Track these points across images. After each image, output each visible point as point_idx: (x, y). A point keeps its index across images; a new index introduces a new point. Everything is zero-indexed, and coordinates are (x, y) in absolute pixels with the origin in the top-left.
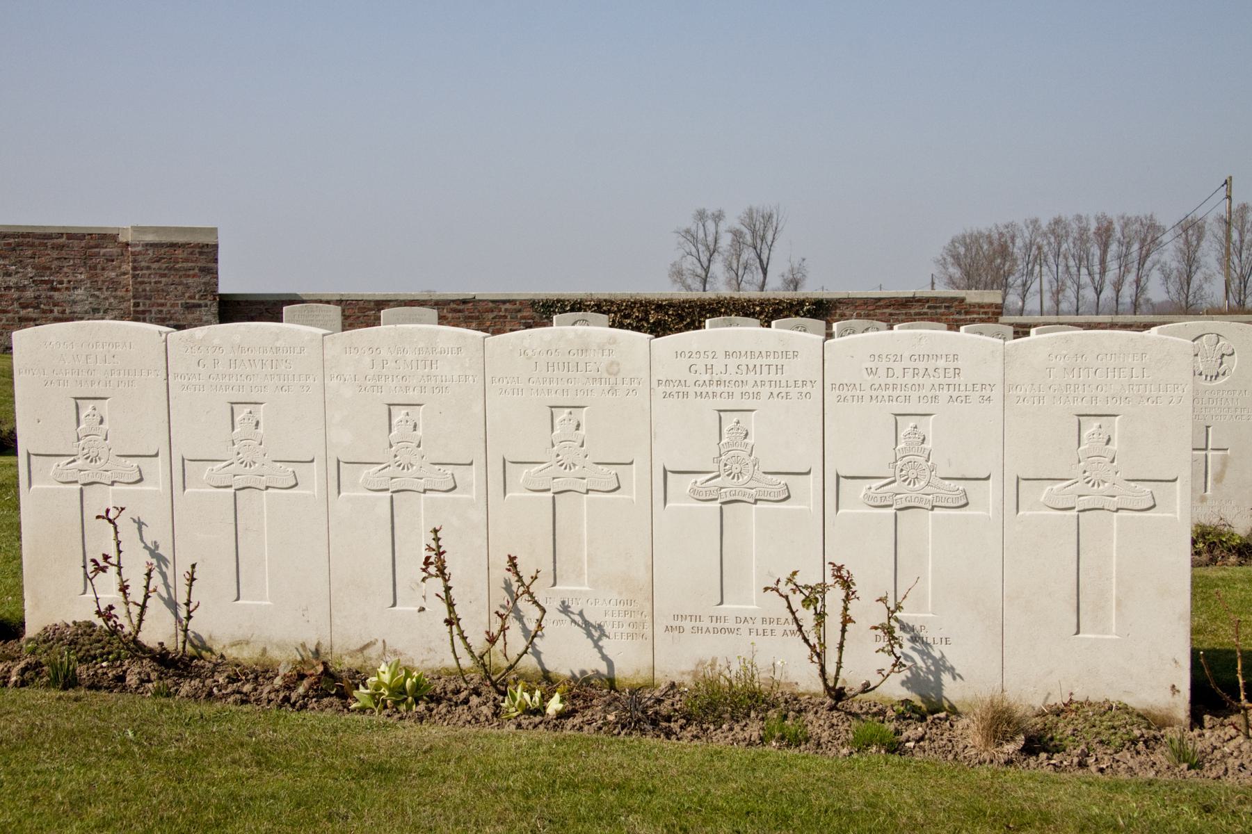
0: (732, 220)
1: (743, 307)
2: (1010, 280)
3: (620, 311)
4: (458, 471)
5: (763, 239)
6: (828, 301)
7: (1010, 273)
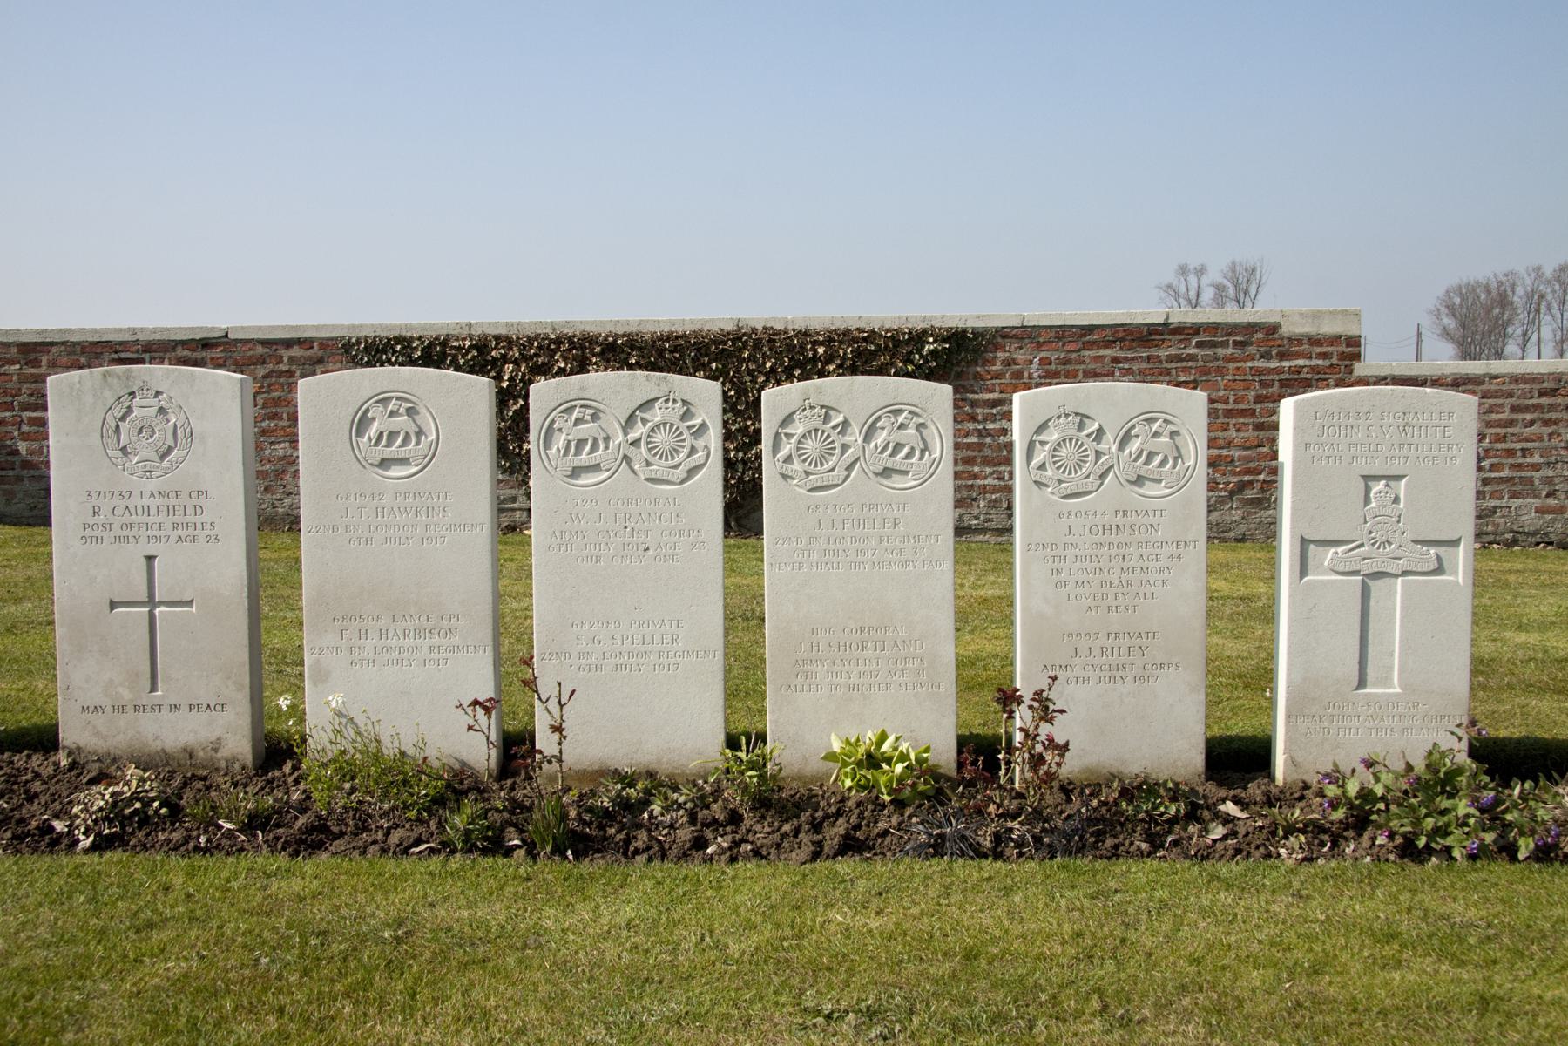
0: (1215, 275)
1: (791, 347)
2: (1510, 330)
3: (525, 358)
4: (1442, 551)
5: (1246, 292)
6: (978, 334)
7: (1509, 322)
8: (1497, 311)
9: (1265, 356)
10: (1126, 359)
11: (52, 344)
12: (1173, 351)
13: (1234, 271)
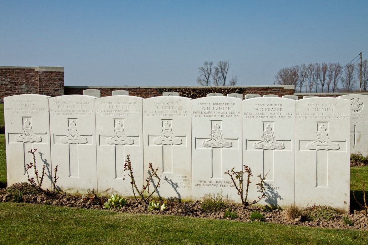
0: (215, 65)
1: (218, 90)
2: (297, 82)
5: (224, 70)
6: (244, 88)
7: (297, 80)
8: (294, 77)
9: (282, 92)
10: (263, 92)
11: (115, 88)
12: (269, 91)
13: (221, 64)
